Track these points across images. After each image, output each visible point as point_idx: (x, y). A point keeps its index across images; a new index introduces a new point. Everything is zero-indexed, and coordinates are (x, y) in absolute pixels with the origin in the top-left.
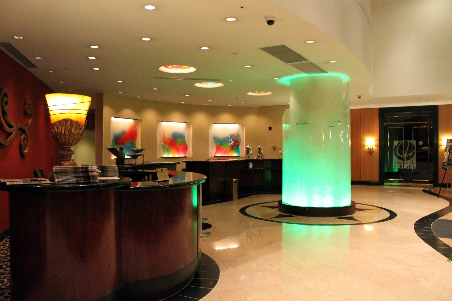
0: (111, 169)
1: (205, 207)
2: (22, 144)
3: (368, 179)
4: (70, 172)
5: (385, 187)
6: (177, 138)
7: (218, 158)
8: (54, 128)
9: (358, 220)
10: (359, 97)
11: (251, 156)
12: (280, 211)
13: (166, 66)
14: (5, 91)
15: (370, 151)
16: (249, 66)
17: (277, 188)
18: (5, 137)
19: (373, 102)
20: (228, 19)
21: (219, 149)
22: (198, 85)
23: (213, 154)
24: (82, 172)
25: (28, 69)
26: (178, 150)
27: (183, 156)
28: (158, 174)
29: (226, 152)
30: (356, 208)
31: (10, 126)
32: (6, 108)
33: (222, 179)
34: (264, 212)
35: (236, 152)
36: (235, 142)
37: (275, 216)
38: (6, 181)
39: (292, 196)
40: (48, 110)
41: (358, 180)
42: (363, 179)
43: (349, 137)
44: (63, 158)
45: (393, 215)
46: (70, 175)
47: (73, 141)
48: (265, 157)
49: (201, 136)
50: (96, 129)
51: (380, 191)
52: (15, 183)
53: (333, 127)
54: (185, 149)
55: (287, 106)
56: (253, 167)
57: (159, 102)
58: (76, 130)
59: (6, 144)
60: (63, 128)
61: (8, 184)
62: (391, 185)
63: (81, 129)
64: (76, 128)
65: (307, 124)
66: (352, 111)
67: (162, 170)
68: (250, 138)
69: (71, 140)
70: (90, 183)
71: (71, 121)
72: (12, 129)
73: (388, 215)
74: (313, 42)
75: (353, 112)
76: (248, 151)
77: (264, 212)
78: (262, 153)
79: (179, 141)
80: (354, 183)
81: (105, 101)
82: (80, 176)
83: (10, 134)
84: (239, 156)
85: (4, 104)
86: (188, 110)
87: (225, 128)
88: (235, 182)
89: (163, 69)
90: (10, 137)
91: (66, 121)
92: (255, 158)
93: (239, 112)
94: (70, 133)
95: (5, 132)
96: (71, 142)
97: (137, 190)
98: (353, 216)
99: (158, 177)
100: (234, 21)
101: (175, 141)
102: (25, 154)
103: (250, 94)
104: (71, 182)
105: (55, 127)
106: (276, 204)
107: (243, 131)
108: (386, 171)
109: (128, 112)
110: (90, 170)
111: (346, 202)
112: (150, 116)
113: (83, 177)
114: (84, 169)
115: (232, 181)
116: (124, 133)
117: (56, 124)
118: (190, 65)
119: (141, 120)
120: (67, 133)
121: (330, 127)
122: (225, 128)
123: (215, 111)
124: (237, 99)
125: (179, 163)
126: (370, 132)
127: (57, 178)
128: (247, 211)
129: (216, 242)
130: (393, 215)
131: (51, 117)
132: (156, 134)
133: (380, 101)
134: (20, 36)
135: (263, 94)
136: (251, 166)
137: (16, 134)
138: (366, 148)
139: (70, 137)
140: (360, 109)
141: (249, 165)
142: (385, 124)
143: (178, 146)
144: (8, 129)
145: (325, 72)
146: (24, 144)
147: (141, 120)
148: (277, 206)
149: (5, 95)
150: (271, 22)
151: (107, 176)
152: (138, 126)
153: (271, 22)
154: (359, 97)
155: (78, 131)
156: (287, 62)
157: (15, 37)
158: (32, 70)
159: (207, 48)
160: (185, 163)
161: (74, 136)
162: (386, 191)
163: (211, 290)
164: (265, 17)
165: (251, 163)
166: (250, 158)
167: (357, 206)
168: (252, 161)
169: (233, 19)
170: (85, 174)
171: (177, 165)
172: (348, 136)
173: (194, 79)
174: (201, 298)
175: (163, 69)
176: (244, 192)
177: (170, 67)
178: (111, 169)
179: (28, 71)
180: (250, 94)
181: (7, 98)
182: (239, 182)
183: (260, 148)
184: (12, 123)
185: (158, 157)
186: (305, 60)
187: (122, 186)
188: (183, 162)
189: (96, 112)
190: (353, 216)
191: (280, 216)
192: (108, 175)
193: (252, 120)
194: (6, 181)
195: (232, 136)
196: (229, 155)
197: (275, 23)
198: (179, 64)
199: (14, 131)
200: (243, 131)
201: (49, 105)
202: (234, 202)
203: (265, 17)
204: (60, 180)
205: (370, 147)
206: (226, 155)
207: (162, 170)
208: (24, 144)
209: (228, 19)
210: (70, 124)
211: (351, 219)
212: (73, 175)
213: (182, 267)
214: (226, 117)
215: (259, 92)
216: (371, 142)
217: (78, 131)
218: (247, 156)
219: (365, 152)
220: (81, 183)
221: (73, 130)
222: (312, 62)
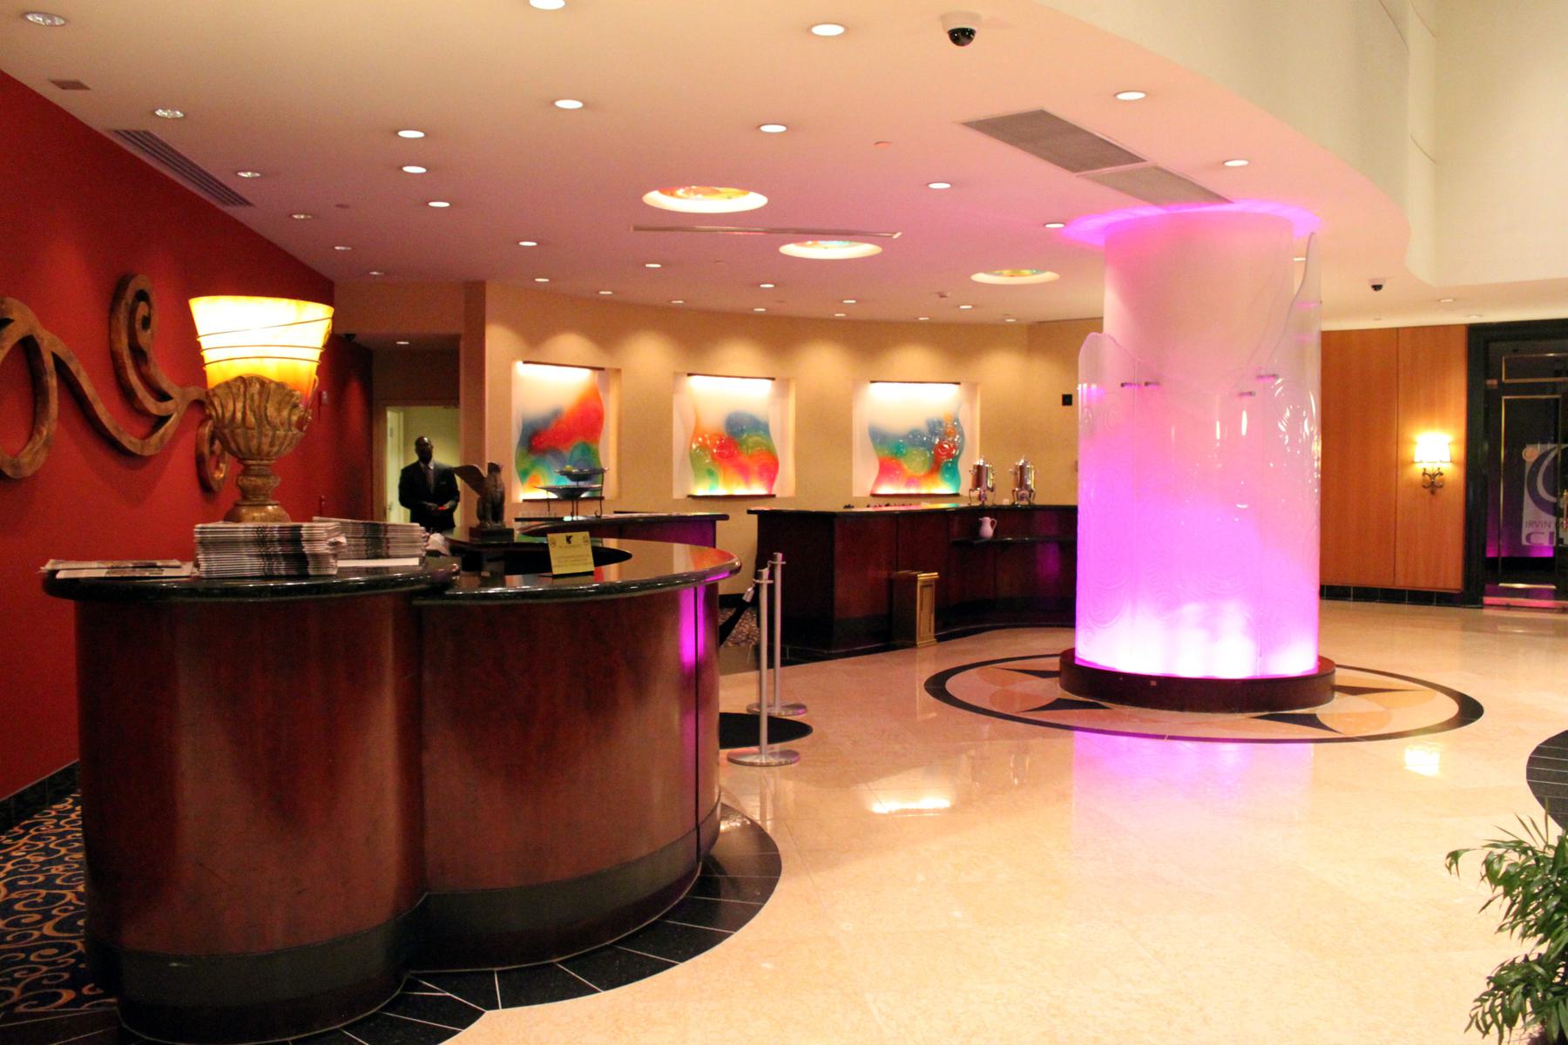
0: (399, 535)
1: (787, 668)
2: (206, 450)
3: (1422, 584)
4: (246, 542)
5: (1487, 612)
6: (742, 431)
7: (883, 501)
8: (212, 404)
9: (1328, 724)
10: (1377, 288)
11: (989, 494)
12: (1066, 687)
13: (668, 188)
14: (141, 282)
15: (1432, 484)
16: (947, 186)
17: (1059, 610)
18: (144, 430)
19: (1436, 302)
20: (820, 30)
21: (887, 469)
22: (791, 249)
23: (864, 486)
24: (281, 541)
25: (219, 206)
26: (744, 473)
27: (763, 491)
28: (554, 554)
29: (911, 481)
30: (1338, 682)
31: (163, 396)
32: (144, 338)
33: (883, 574)
34: (1010, 688)
35: (948, 480)
36: (939, 449)
37: (1044, 703)
38: (60, 566)
39: (1118, 641)
40: (197, 347)
41: (1352, 580)
42: (1401, 583)
43: (1316, 429)
44: (245, 498)
45: (1469, 710)
46: (244, 551)
47: (272, 445)
48: (1039, 500)
49: (826, 427)
50: (462, 400)
51: (1464, 629)
52: (83, 574)
53: (1250, 394)
54: (770, 469)
55: (1096, 323)
56: (995, 532)
57: (677, 309)
58: (279, 411)
59: (147, 453)
60: (239, 405)
61: (60, 576)
62: (1508, 607)
63: (295, 406)
64: (280, 403)
65: (1157, 384)
66: (1326, 337)
67: (568, 539)
68: (998, 429)
69: (266, 441)
70: (306, 577)
71: (263, 382)
72: (170, 405)
73: (1452, 709)
74: (1141, 95)
75: (1333, 344)
76: (979, 475)
77: (1010, 688)
78: (1027, 487)
79: (752, 439)
80: (1329, 592)
81: (490, 306)
82: (276, 555)
83: (162, 420)
84: (956, 495)
85: (138, 326)
86: (780, 334)
87: (909, 397)
88: (927, 584)
89: (655, 198)
90: (162, 431)
91: (244, 381)
92: (1006, 502)
93: (959, 341)
94: (262, 418)
95: (143, 413)
96: (266, 448)
97: (488, 603)
98: (1320, 711)
99: (554, 562)
100: (839, 36)
101: (734, 444)
102: (215, 487)
103: (980, 277)
104: (248, 574)
105: (216, 403)
106: (1054, 664)
107: (972, 408)
108: (1490, 555)
109: (571, 344)
110: (305, 537)
111: (1296, 661)
112: (648, 356)
113: (286, 557)
114: (287, 534)
115: (915, 579)
116: (556, 414)
117: (219, 392)
118: (746, 186)
119: (618, 371)
120: (251, 419)
121: (1242, 394)
122: (909, 397)
123: (871, 340)
124: (942, 296)
125: (725, 517)
126: (1431, 409)
127: (206, 560)
128: (952, 685)
129: (863, 787)
130: (1469, 710)
131: (209, 369)
132: (669, 419)
133: (1461, 299)
134: (173, 110)
135: (1028, 277)
136: (988, 529)
137: (183, 421)
138: (1417, 470)
139: (261, 434)
140: (1398, 329)
141: (980, 524)
142: (1489, 382)
143: (743, 459)
144: (152, 405)
145: (1228, 201)
146: (212, 453)
147: (618, 371)
148: (1057, 668)
149: (142, 296)
150: (961, 36)
151: (388, 557)
152: (607, 390)
153: (961, 36)
154: (1377, 288)
155: (285, 413)
156: (1074, 170)
157: (160, 112)
158: (231, 210)
159: (781, 129)
160: (755, 517)
161: (275, 428)
162: (1492, 627)
163: (728, 936)
164: (943, 18)
165: (988, 520)
166: (988, 503)
167: (1341, 677)
168: (996, 512)
169: (836, 30)
170: (290, 549)
171: (719, 523)
172: (1310, 429)
173: (784, 231)
174: (682, 960)
175: (655, 198)
176: (959, 619)
177: (680, 192)
178: (399, 535)
179: (224, 214)
180: (980, 277)
181: (150, 306)
182: (939, 587)
183: (1022, 468)
184: (166, 384)
185: (678, 494)
186: (1134, 159)
187: (417, 587)
188: (750, 512)
189: (462, 343)
190: (1320, 711)
191: (1058, 704)
192: (391, 552)
193: (1005, 371)
194: (60, 566)
195: (935, 427)
196: (924, 491)
197: (976, 38)
198: (710, 180)
199: (175, 409)
200: (972, 408)
201: (200, 332)
202: (920, 653)
203: (943, 18)
204: (215, 566)
205: (1431, 469)
206: (913, 491)
207: (568, 539)
208: (212, 453)
209: (820, 30)
210: (260, 393)
211: (1311, 721)
212: (254, 550)
213: (644, 851)
214: (914, 358)
215: (1016, 266)
216: (1435, 447)
217: (285, 413)
218: (976, 493)
219: (1411, 484)
220: (280, 577)
221: (271, 411)
222: (1163, 164)
